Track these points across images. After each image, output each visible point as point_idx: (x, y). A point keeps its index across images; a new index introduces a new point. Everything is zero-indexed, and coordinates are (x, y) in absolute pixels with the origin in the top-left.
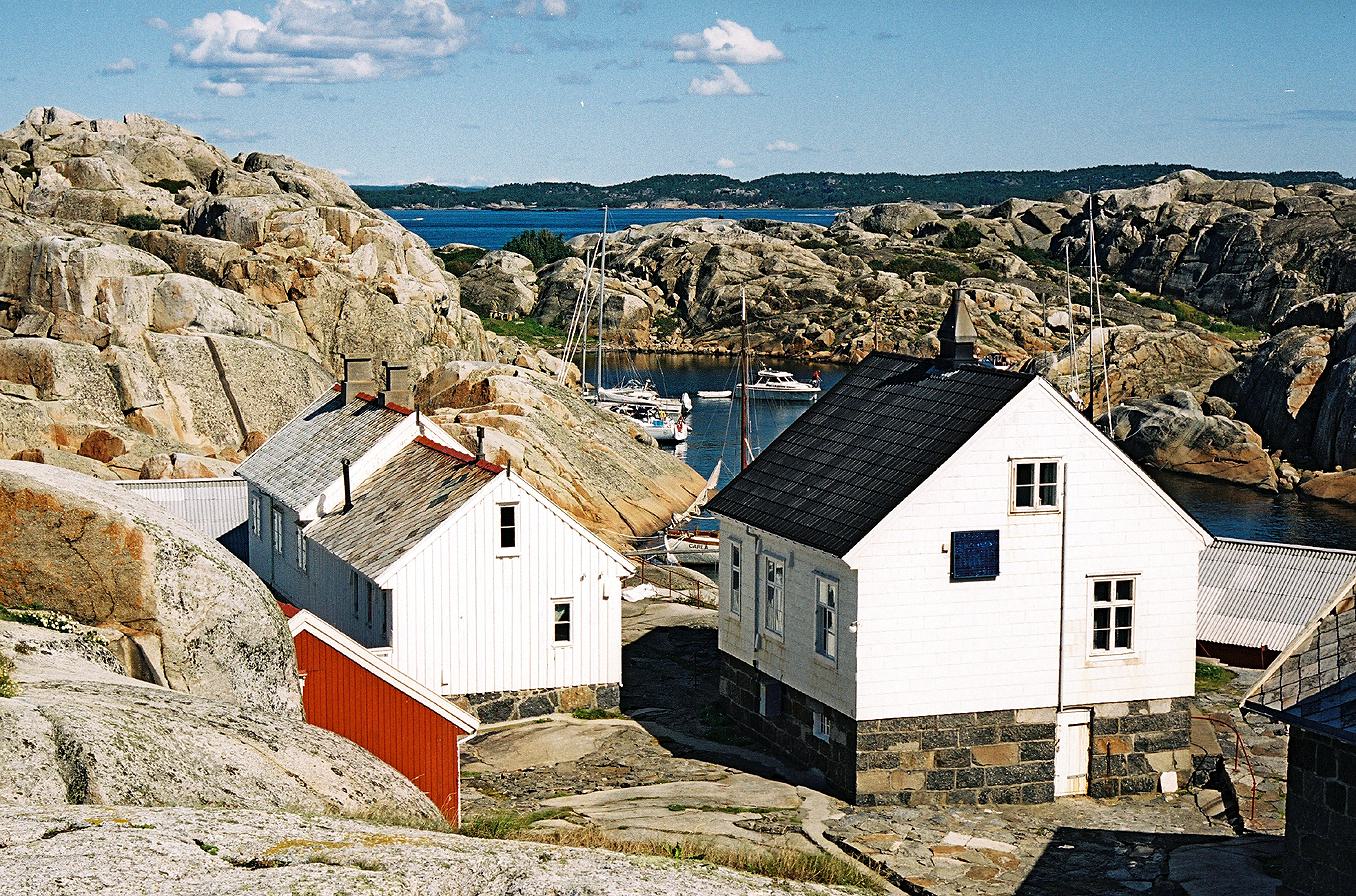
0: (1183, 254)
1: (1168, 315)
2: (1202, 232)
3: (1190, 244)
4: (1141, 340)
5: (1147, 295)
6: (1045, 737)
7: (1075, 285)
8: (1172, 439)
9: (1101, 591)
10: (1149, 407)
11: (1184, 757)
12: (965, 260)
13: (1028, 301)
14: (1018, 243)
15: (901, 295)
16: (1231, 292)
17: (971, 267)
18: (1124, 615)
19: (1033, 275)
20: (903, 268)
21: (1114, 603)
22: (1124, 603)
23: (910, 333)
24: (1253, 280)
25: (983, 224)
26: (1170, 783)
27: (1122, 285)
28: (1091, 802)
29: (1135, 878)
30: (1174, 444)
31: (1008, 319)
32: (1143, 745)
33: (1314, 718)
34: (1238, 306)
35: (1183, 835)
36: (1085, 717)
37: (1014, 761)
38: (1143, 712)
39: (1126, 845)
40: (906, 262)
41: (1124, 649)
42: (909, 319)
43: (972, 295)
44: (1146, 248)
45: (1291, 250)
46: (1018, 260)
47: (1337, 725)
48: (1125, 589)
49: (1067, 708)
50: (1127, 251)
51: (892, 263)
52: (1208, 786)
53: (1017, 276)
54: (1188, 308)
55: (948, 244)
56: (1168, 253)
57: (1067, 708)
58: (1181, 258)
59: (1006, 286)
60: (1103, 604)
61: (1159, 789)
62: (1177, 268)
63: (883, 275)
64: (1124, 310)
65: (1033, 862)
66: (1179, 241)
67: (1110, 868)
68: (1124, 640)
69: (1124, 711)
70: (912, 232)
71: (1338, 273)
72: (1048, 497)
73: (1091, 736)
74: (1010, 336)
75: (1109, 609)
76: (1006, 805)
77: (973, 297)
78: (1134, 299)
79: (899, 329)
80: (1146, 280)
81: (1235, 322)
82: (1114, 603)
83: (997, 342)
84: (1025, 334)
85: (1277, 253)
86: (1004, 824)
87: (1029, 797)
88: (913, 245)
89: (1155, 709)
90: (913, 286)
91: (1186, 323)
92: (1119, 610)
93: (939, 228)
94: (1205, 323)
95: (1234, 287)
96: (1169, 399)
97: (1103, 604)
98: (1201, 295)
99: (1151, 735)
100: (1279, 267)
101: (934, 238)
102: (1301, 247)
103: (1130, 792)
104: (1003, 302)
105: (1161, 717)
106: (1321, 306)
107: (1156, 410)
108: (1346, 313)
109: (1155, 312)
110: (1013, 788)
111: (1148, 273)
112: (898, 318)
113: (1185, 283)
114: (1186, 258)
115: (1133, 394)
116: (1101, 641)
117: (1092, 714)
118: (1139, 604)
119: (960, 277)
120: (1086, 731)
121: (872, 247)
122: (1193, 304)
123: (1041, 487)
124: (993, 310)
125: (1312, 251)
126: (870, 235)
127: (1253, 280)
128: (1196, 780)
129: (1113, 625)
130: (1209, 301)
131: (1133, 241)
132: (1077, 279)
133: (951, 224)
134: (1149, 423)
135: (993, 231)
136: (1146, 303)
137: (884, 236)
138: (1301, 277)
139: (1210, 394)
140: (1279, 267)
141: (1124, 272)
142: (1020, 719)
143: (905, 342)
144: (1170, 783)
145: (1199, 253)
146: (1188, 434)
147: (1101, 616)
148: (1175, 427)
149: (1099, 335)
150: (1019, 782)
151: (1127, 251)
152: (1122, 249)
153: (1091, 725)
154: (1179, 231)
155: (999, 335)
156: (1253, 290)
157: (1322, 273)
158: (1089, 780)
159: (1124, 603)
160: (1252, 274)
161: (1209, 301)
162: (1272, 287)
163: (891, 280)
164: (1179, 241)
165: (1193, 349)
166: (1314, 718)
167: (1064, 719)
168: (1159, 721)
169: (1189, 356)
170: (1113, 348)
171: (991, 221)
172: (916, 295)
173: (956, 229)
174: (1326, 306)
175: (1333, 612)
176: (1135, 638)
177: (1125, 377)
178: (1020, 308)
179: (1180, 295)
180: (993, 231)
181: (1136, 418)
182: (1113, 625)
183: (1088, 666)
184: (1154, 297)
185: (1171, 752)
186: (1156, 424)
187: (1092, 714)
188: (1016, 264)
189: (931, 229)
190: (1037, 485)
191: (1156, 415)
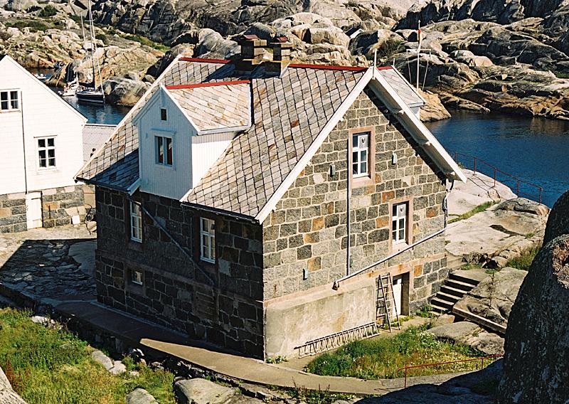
0: (143, 16)
1: (137, 43)
2: (151, 7)
3: (146, 12)
4: (117, 52)
5: (128, 34)
6: (21, 204)
7: (97, 31)
8: (128, 93)
9: (41, 143)
10: (118, 80)
11: (82, 210)
12: (49, 22)
13: (76, 39)
14: (73, 14)
15: (18, 37)
16: (163, 32)
17: (51, 25)
18: (52, 153)
19: (78, 27)
20: (19, 25)
21: (47, 148)
22: (51, 148)
23: (22, 54)
24: (172, 27)
25: (57, 6)
26: (76, 220)
27: (117, 30)
28: (44, 229)
29: (54, 256)
30: (129, 95)
31: (66, 47)
32: (64, 205)
33: (100, 181)
34: (167, 38)
35: (78, 239)
36: (39, 195)
37: (9, 215)
38: (63, 192)
39: (53, 244)
40: (21, 23)
41: (44, 168)
42: (21, 48)
43: (50, 36)
44: (127, 14)
45: (188, 13)
46: (72, 21)
47: (107, 182)
48: (51, 142)
49: (29, 192)
50: (119, 16)
51: (16, 24)
52: (93, 220)
53: (71, 28)
54: (146, 40)
55: (42, 15)
56: (137, 16)
57: (29, 192)
58: (142, 19)
59: (65, 32)
60: (42, 149)
61: (72, 223)
62: (141, 23)
63: (10, 29)
64: (118, 41)
65: (13, 253)
66: (141, 12)
67: (44, 253)
68: (52, 163)
69: (54, 192)
70: (26, 10)
71: (207, 23)
72: (14, 105)
73: (42, 203)
74: (67, 54)
75: (44, 151)
76: (7, 233)
77: (51, 38)
78: (123, 36)
79: (18, 52)
80: (128, 28)
81: (165, 45)
82: (47, 148)
83: (61, 56)
84: (73, 53)
85: (182, 15)
86: (5, 240)
87: (16, 229)
88: (25, 16)
89: (67, 190)
90: (24, 33)
91: (144, 46)
92: (49, 151)
93: (37, 8)
94: (153, 46)
95: (164, 30)
96: (127, 77)
97: (42, 149)
98: (151, 34)
99: (66, 201)
100: (183, 21)
101: (35, 12)
102: (192, 13)
103: (59, 225)
104: (64, 39)
105: (71, 194)
106: (190, 35)
107: (121, 81)
108: (200, 37)
109: (131, 42)
110: (9, 226)
111: (129, 25)
112: (17, 47)
113: (145, 29)
114: (145, 18)
115: (115, 75)
116: (43, 164)
117: (42, 194)
118: (57, 147)
119: (45, 29)
120: (39, 200)
121: (7, 17)
122: (148, 38)
123: (6, 99)
124: (59, 43)
125: (196, 14)
126: (7, 12)
127: (172, 27)
128: (88, 218)
129: (47, 156)
130: (154, 36)
131: (122, 12)
132: (98, 28)
133: (43, 6)
134: (119, 86)
135: (62, 9)
136: (127, 38)
137: (13, 12)
138: (192, 25)
139: (147, 74)
140: (183, 21)
141: (118, 25)
142: (10, 198)
143: (20, 58)
144: (76, 220)
145: (149, 16)
146: (135, 90)
147: (42, 154)
148: (129, 88)
149: (100, 51)
150: (12, 223)
151: (119, 16)
152: (117, 15)
153: (41, 199)
154: (141, 6)
155: (62, 54)
156: (173, 31)
157: (201, 23)
158: (43, 221)
159: (51, 148)
160: (172, 24)
161: (154, 36)
162: (180, 29)
163: (14, 32)
164: (141, 12)
165: (140, 55)
166: (100, 181)
167: (29, 197)
168: (70, 195)
169: (139, 58)
170: (106, 56)
171: (60, 5)
172: (24, 37)
173: (45, 9)
174: (192, 34)
175: (111, 140)
176: (57, 162)
177: (111, 69)
178: (72, 42)
179: (143, 34)
180: (62, 9)
181: (113, 84)
182: (47, 156)
183: (38, 174)
184: (132, 35)
185: (75, 208)
186: (122, 87)
187: (42, 194)
188: (71, 23)
189: (34, 9)
190: (9, 100)
191: (121, 83)
